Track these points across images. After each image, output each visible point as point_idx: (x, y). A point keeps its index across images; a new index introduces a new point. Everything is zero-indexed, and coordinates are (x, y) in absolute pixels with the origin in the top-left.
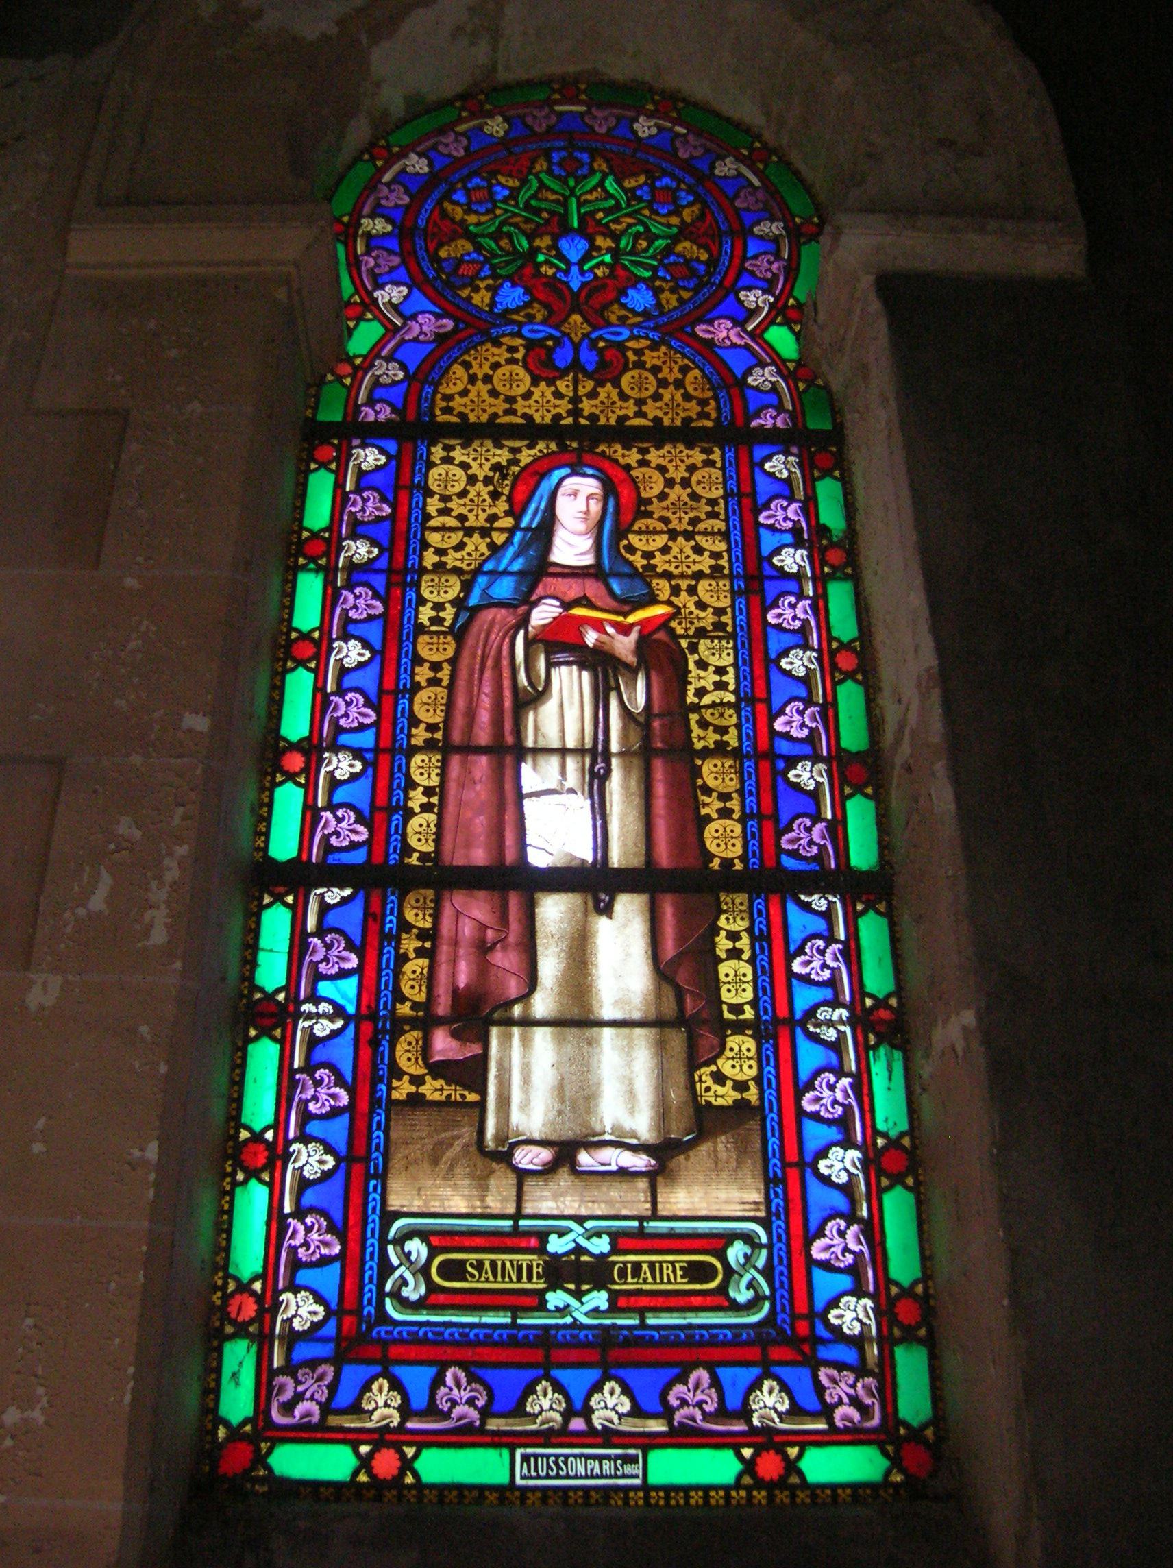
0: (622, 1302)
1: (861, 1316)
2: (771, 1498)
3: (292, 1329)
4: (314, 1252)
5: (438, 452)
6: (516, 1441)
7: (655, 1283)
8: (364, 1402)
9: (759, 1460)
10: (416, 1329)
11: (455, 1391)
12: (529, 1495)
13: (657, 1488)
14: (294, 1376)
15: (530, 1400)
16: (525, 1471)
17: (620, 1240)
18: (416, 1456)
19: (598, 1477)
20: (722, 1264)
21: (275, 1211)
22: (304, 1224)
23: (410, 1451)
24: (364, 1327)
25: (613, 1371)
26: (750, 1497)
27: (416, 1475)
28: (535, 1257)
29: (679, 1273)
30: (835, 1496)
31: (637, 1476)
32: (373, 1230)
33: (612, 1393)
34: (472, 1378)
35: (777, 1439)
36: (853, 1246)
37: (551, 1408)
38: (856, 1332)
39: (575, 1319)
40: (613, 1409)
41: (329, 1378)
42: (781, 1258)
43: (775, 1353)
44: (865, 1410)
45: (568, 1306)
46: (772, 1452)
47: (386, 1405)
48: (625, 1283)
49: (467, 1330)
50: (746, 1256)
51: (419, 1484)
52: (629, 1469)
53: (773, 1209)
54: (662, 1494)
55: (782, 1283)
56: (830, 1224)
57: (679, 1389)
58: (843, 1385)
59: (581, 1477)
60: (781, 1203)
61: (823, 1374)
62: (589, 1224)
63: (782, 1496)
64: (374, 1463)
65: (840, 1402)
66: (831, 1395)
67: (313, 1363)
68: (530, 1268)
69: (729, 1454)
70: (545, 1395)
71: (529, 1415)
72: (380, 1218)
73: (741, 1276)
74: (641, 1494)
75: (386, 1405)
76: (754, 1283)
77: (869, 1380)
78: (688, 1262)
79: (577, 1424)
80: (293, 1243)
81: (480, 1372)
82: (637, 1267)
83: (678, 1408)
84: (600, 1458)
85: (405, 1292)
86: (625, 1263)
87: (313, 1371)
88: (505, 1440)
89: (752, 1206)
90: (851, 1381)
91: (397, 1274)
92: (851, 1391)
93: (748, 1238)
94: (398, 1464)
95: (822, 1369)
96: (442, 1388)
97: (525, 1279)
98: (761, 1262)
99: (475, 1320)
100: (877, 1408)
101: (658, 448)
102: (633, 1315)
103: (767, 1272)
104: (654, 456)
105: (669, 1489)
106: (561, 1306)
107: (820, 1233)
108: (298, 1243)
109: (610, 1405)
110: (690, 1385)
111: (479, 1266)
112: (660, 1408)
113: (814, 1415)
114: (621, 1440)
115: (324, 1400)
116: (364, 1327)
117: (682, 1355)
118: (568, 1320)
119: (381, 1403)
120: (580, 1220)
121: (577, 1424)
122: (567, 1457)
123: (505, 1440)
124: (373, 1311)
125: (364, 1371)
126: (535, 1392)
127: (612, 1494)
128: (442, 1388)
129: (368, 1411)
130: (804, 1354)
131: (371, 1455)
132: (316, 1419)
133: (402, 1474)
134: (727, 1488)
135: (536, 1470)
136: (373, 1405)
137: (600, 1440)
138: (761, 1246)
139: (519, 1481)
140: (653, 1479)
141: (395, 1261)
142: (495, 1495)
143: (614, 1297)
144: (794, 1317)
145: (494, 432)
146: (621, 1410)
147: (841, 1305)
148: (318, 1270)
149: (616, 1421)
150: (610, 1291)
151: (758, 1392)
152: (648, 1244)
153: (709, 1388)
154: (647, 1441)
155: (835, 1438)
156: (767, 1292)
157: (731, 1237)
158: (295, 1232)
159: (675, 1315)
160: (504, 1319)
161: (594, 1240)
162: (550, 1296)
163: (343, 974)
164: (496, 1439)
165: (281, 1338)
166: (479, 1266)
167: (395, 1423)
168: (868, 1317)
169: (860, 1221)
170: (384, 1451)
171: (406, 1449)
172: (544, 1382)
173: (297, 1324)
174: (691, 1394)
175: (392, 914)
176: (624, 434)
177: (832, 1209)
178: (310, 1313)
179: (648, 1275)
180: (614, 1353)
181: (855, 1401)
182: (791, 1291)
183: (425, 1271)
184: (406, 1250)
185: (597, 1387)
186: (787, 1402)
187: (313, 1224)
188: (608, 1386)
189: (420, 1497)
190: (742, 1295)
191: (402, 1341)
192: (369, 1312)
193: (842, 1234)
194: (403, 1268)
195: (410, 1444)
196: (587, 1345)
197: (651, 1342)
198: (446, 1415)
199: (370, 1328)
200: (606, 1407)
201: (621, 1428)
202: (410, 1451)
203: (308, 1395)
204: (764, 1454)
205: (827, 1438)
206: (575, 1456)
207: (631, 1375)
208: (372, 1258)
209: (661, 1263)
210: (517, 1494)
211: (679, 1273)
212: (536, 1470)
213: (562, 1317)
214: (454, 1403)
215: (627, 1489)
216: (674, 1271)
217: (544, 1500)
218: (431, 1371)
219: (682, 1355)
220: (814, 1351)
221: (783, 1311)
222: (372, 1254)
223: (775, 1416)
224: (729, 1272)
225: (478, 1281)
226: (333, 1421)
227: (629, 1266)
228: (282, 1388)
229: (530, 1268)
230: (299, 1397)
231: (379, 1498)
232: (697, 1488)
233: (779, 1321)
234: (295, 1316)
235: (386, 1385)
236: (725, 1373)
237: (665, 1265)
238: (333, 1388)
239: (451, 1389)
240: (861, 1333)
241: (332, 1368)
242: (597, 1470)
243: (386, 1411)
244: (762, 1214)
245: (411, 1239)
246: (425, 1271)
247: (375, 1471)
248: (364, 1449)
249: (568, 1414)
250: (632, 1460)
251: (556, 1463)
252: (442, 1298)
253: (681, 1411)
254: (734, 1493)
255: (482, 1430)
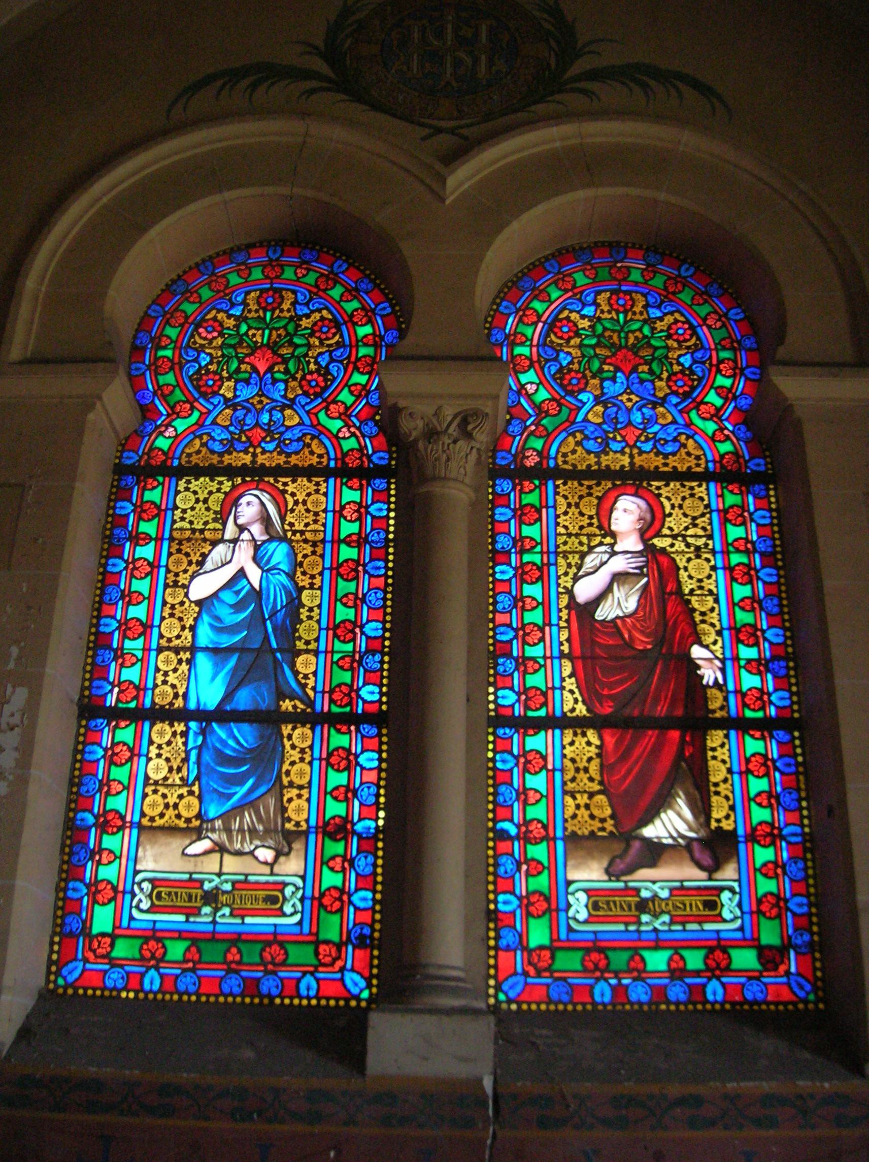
5: (182, 485)
82: (190, 900)
101: (311, 465)
104: (315, 460)
111: (169, 894)
145: (212, 472)
176: (277, 471)
246: (150, 896)
252: (714, 892)
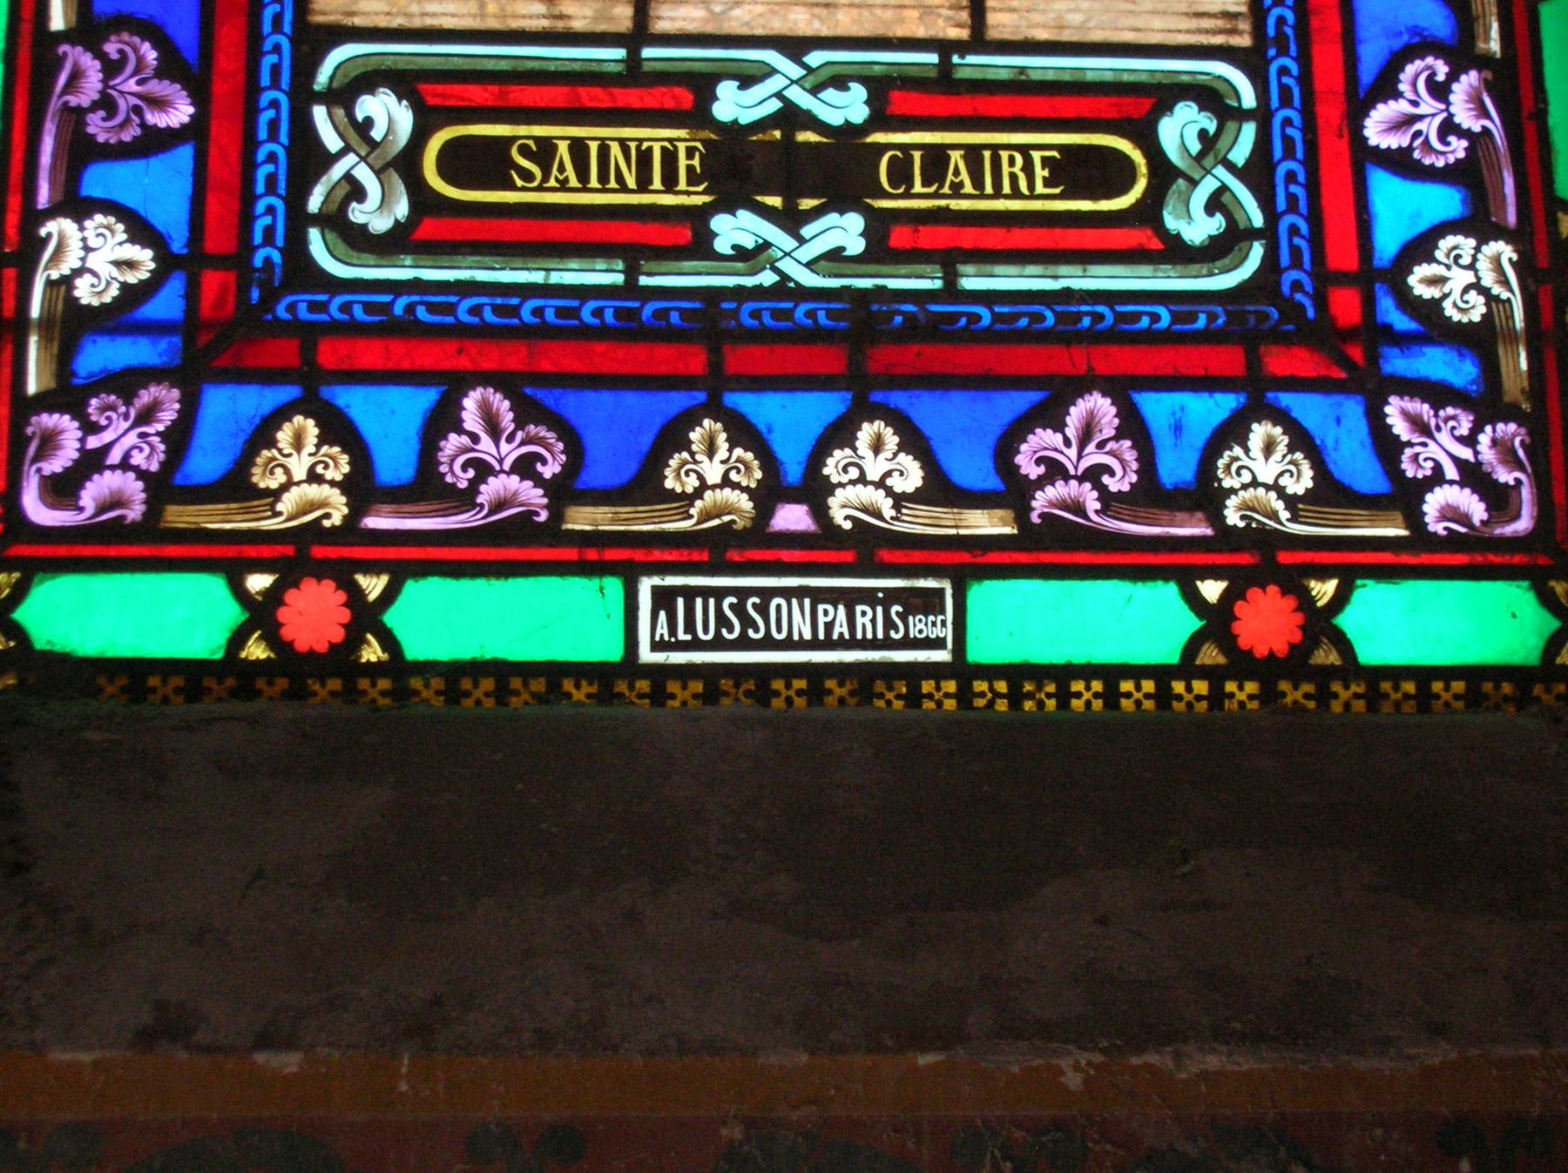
0: (900, 237)
1: (1488, 280)
2: (1268, 696)
3: (72, 302)
4: (127, 120)
6: (639, 555)
7: (983, 196)
8: (257, 471)
9: (1240, 608)
10: (387, 298)
11: (486, 443)
12: (673, 687)
13: (990, 672)
14: (79, 413)
15: (674, 462)
16: (662, 630)
17: (896, 95)
18: (389, 596)
19: (842, 644)
20: (1147, 154)
21: (26, 28)
22: (101, 56)
23: (373, 586)
24: (255, 295)
25: (877, 397)
26: (1217, 697)
27: (389, 640)
28: (682, 133)
29: (1041, 173)
30: (1424, 698)
31: (939, 644)
32: (276, 70)
33: (877, 447)
34: (527, 412)
35: (1284, 557)
36: (1465, 118)
37: (726, 482)
38: (1476, 316)
39: (785, 277)
40: (880, 484)
41: (168, 416)
42: (1288, 142)
43: (1277, 361)
44: (1499, 499)
45: (766, 245)
46: (1273, 589)
47: (313, 477)
48: (907, 195)
49: (515, 301)
50: (1203, 134)
51: (397, 664)
52: (919, 626)
53: (1271, 32)
54: (1002, 686)
55: (1292, 199)
56: (1410, 69)
57: (1044, 439)
58: (1444, 437)
59: (802, 645)
60: (1290, 16)
61: (1395, 413)
62: (815, 58)
63: (1293, 693)
64: (283, 614)
65: (1437, 478)
66: (1415, 457)
67: (125, 383)
68: (669, 158)
69: (1167, 593)
70: (711, 451)
71: (671, 496)
72: (293, 41)
73: (1194, 183)
74: (950, 686)
75: (313, 477)
76: (1226, 198)
77: (1507, 429)
78: (1060, 148)
79: (792, 518)
80: (73, 101)
81: (547, 397)
82: (936, 159)
83: (1041, 483)
84: (850, 598)
85: (358, 214)
86: (906, 148)
87: (128, 403)
88: (613, 554)
89: (1220, 23)
90: (1464, 430)
91: (338, 171)
92: (1465, 453)
93: (1210, 97)
94: (345, 615)
95: (1393, 400)
96: (453, 437)
97: (657, 183)
98: (1242, 151)
99: (537, 277)
100: (1526, 493)
102: (927, 268)
103: (1258, 173)
105: (1016, 674)
106: (749, 244)
107: (1386, 87)
108: (85, 101)
109: (873, 474)
110: (1071, 432)
112: (993, 482)
113: (1372, 504)
114: (898, 557)
115: (154, 467)
116: (255, 295)
117: (1057, 361)
118: (767, 278)
119: (299, 473)
120: (794, 47)
121: (792, 518)
122: (767, 594)
123: (613, 554)
124: (276, 257)
125: (253, 401)
126: (686, 445)
127: (880, 686)
128: (453, 437)
129: (267, 492)
130: (1347, 364)
131: (274, 596)
132: (135, 513)
133: (354, 640)
134: (1161, 674)
135: (690, 627)
136: (280, 478)
137: (848, 556)
138: (1242, 115)
139: (646, 655)
140: (980, 651)
141: (331, 141)
142: (586, 688)
143: (878, 227)
144: (1324, 278)
146: (899, 485)
147: (1439, 255)
148: (138, 166)
149: (888, 512)
150: (871, 215)
151: (1238, 451)
152: (963, 105)
153: (1117, 438)
154: (965, 557)
155: (1424, 559)
156: (1258, 220)
157: (1166, 95)
158: (77, 75)
159: (1032, 269)
160: (606, 275)
161: (830, 94)
162: (719, 222)
163: (154, 143)
164: (592, 555)
165: (46, 324)
166: (543, 152)
167: (336, 519)
168: (1505, 283)
169: (1482, 62)
170: (310, 587)
171: (363, 580)
172: (707, 422)
173: (84, 291)
174: (1072, 452)
175: (275, 85)
177: (1415, 31)
178: (118, 264)
179: (964, 176)
180: (882, 356)
181: (1473, 476)
182: (1315, 218)
183: (407, 164)
184: (360, 117)
185: (839, 433)
186: (1308, 473)
187: (121, 51)
188: (866, 433)
189: (401, 694)
190: (1198, 227)
191: (352, 329)
192: (267, 260)
193: (1440, 91)
194: (351, 159)
195: (372, 568)
196: (812, 335)
197: (974, 335)
198: (466, 499)
199: (271, 297)
200: (862, 480)
201: (899, 527)
202: (373, 586)
203: (115, 457)
204: (1254, 593)
205: (1407, 559)
206: (787, 593)
207: (926, 409)
208: (273, 136)
209: (995, 148)
210: (643, 685)
211: (1041, 173)
212: (690, 627)
213: (753, 273)
214: (483, 470)
215: (914, 672)
216: (1028, 168)
217: (711, 696)
218: (425, 398)
219: (1057, 361)
220: (1374, 359)
221: (1296, 262)
222: (274, 125)
223: (1279, 506)
224: (1164, 173)
225: (540, 189)
226: (179, 516)
227: (917, 155)
228: (50, 442)
229: (669, 158)
230: (92, 462)
231: (298, 693)
232: (1088, 672)
233: (1286, 289)
234: (78, 273)
235: (311, 429)
236: (1157, 407)
237: (1004, 155)
238: (179, 439)
239: (475, 438)
240: (1487, 318)
241: (176, 393)
242: (842, 628)
243: (314, 491)
244: (1244, 41)
245: (371, 90)
246: (407, 164)
247: (287, 633)
248: (258, 582)
249: (768, 495)
250: (929, 603)
251: (739, 609)
253: (1050, 490)
254: (1178, 687)
255: (553, 532)
